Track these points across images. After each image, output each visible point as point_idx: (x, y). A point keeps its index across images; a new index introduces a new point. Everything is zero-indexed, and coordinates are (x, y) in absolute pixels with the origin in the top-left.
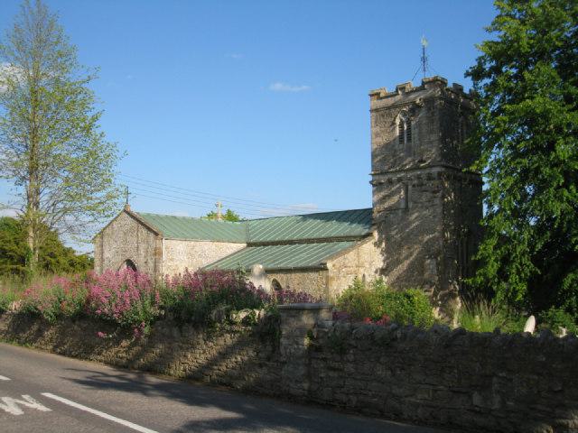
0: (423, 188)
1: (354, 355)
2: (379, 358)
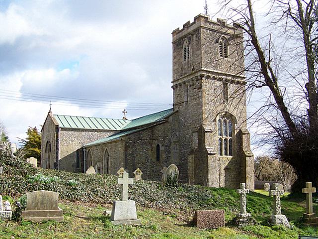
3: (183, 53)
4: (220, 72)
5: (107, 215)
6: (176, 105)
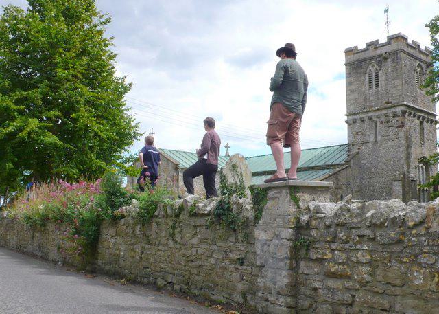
0: (390, 124)
1: (371, 252)
2: (416, 256)
3: (367, 80)
4: (418, 107)
5: (240, 239)
6: (353, 145)
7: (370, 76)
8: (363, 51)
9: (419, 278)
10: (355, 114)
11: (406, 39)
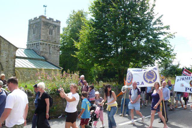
7: (50, 30)
8: (47, 19)
9: (133, 25)
10: (44, 41)
11: (53, 19)
